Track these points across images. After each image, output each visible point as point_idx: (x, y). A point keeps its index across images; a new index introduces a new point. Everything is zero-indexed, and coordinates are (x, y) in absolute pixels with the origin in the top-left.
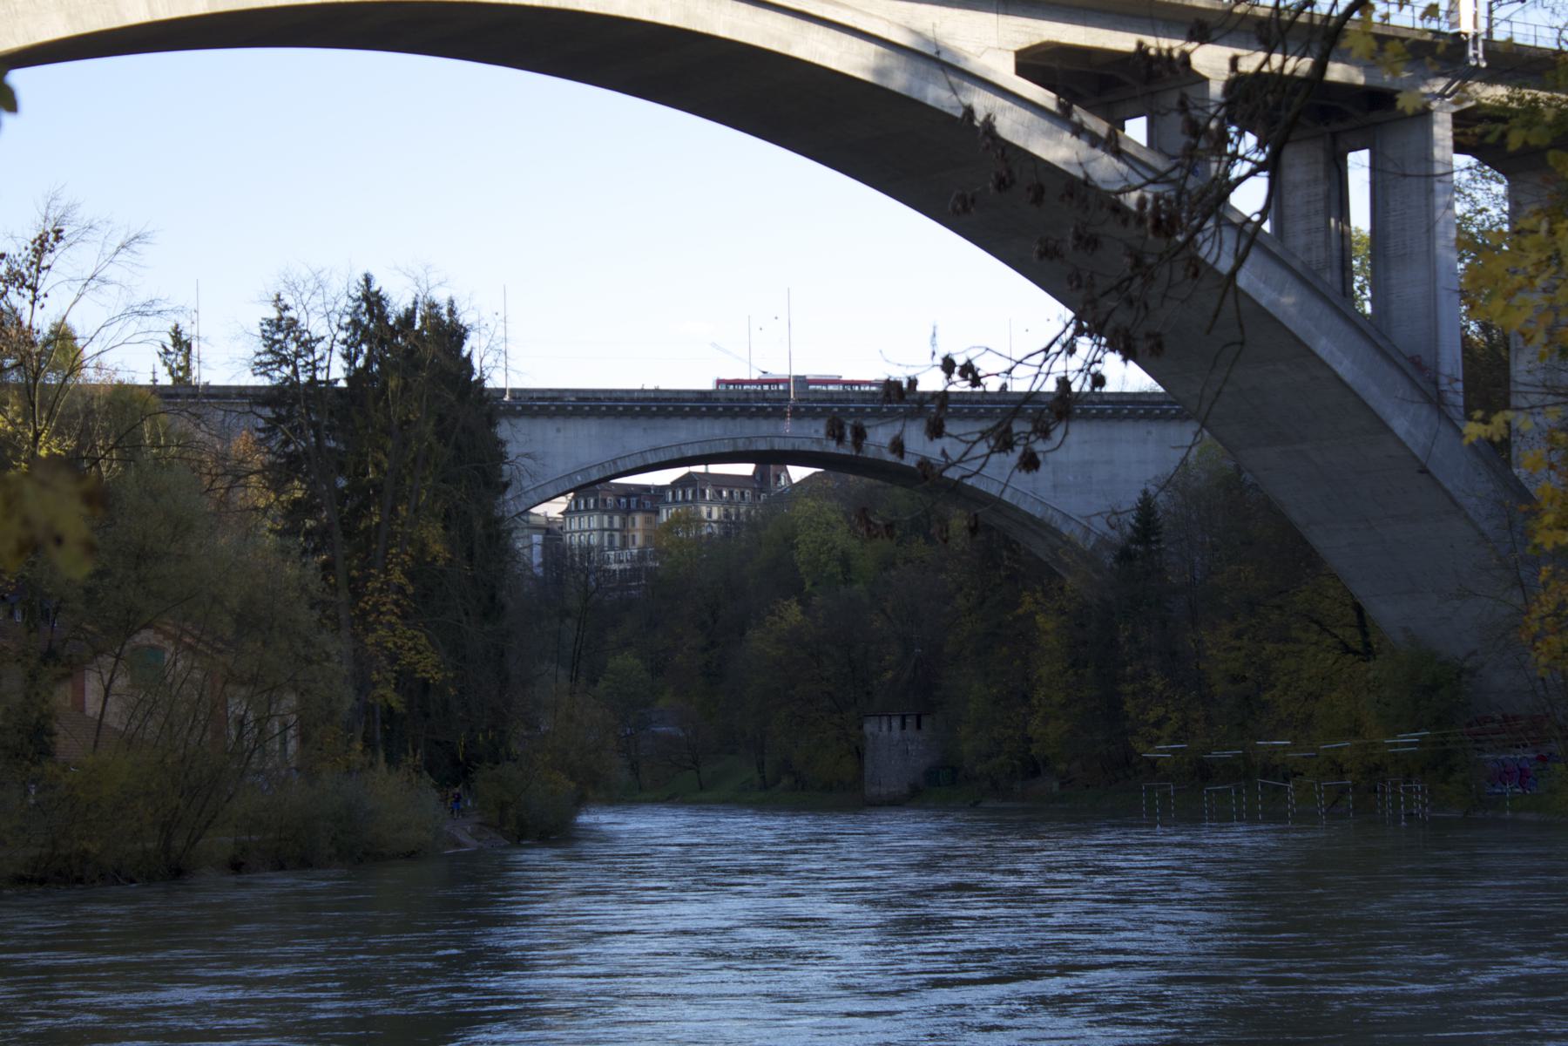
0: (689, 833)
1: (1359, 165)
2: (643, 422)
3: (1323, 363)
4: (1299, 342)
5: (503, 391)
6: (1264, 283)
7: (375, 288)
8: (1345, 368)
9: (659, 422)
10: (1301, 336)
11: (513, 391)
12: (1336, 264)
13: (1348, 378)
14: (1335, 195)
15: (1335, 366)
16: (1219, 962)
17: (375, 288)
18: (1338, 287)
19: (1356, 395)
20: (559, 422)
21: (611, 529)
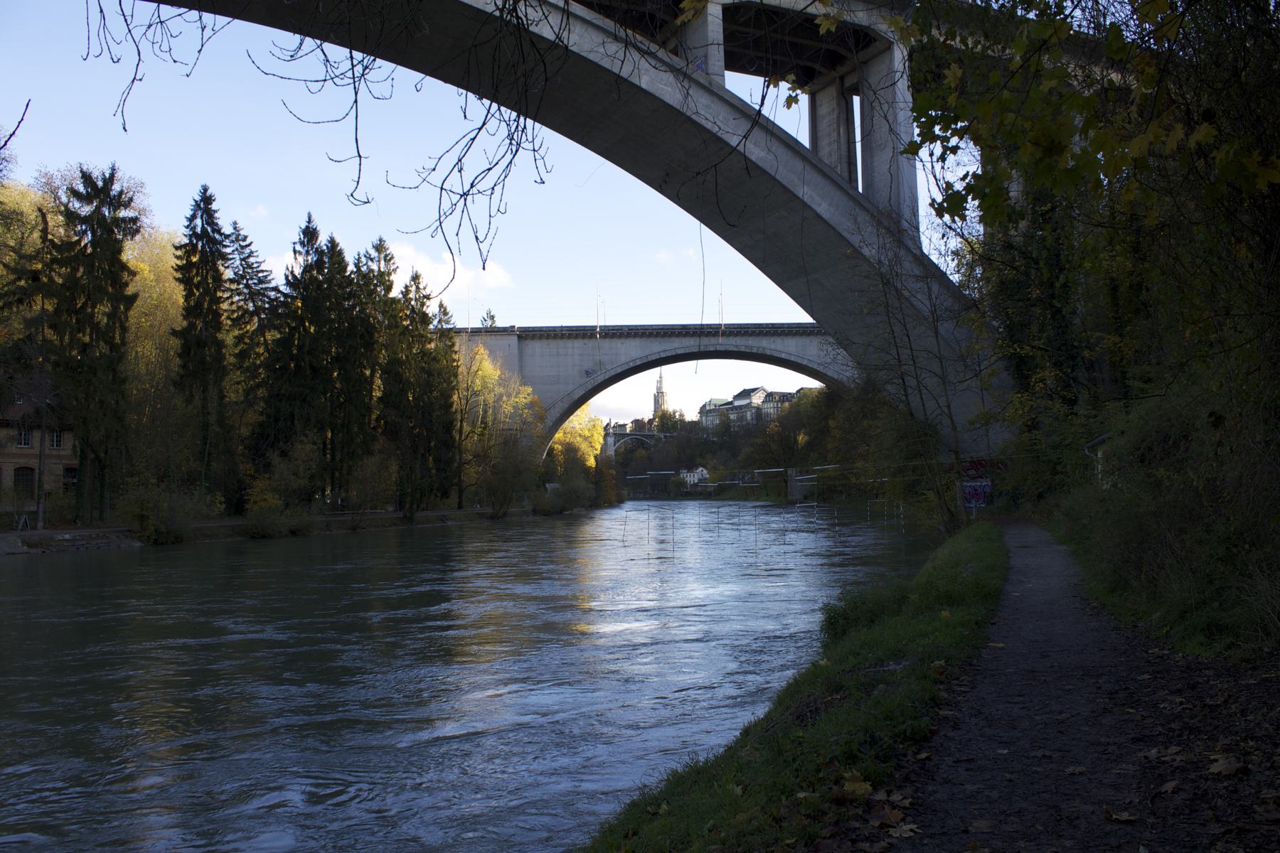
0: (732, 529)
1: (856, 100)
2: (659, 339)
3: (805, 205)
4: (786, 189)
5: (596, 327)
6: (755, 144)
7: (208, 193)
8: (823, 208)
9: (666, 339)
10: (785, 183)
11: (600, 327)
12: (845, 160)
13: (825, 215)
14: (843, 116)
15: (814, 206)
16: (554, 759)
17: (208, 193)
18: (846, 175)
19: (833, 228)
20: (623, 340)
21: (777, 407)
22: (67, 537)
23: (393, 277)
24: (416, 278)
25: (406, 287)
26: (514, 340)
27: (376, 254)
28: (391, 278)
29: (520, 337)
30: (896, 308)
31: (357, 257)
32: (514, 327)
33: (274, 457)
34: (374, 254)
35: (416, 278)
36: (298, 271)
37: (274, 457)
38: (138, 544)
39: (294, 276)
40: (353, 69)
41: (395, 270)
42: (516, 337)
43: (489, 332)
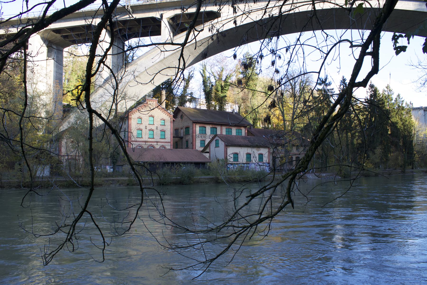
22: (324, 175)
23: (392, 96)
24: (399, 96)
25: (396, 99)
26: (422, 112)
27: (387, 89)
28: (392, 96)
29: (424, 110)
30: (12, 64)
31: (134, 70)
32: (422, 107)
33: (371, 154)
34: (386, 89)
35: (399, 96)
36: (369, 98)
37: (371, 154)
38: (340, 177)
39: (367, 99)
40: (296, 45)
41: (393, 94)
42: (423, 111)
43: (26, 55)
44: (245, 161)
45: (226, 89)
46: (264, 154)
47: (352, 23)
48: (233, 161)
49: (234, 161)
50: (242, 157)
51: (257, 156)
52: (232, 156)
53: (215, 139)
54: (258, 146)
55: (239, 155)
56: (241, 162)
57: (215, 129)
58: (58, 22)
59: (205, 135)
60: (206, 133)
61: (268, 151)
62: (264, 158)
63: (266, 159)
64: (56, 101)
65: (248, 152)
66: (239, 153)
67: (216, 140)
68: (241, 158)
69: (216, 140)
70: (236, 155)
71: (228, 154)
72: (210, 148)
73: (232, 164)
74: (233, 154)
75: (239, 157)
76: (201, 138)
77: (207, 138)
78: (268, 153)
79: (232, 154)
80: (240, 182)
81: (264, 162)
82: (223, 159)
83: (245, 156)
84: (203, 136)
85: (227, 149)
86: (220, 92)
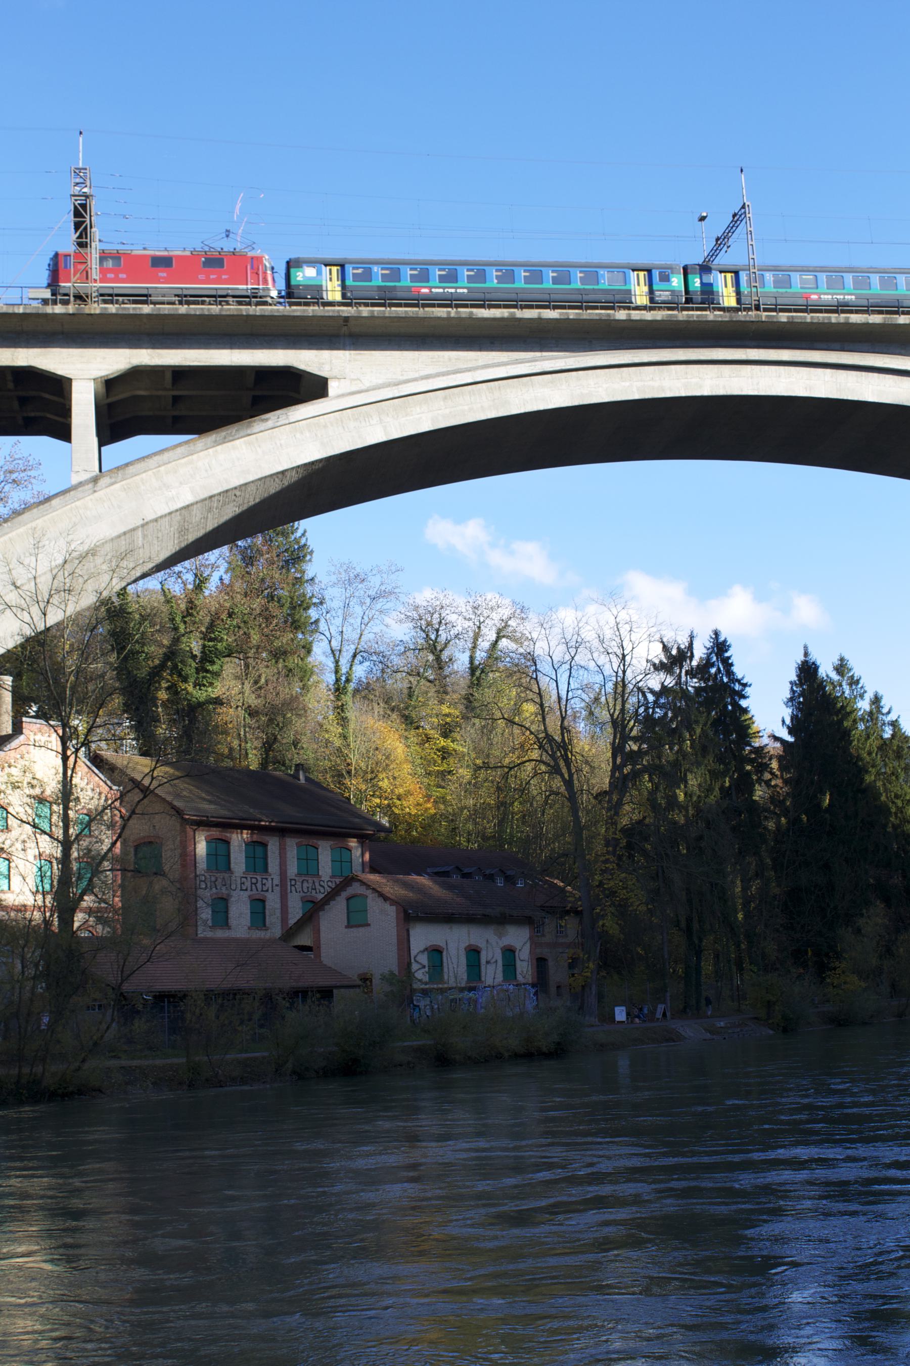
22: (722, 1024)
44: (465, 977)
45: (215, 668)
46: (518, 947)
47: (78, 287)
48: (426, 978)
49: (431, 980)
50: (455, 960)
51: (499, 956)
52: (424, 959)
53: (344, 895)
54: (501, 920)
55: (444, 953)
56: (452, 983)
57: (259, 850)
58: (121, 370)
59: (226, 875)
60: (228, 869)
61: (531, 938)
62: (518, 963)
63: (525, 969)
64: (617, 749)
65: (472, 943)
66: (445, 947)
67: (348, 899)
68: (450, 967)
69: (348, 899)
70: (436, 952)
71: (413, 953)
72: (317, 932)
73: (425, 992)
74: (426, 953)
75: (445, 964)
76: (255, 892)
77: (233, 887)
78: (528, 945)
79: (423, 952)
80: (517, 1056)
81: (520, 978)
82: (392, 973)
83: (463, 960)
84: (220, 880)
85: (408, 931)
86: (192, 680)
